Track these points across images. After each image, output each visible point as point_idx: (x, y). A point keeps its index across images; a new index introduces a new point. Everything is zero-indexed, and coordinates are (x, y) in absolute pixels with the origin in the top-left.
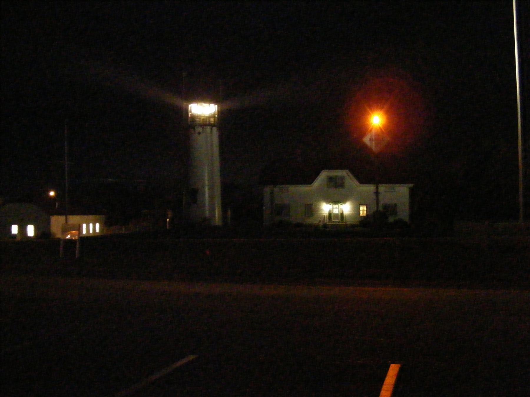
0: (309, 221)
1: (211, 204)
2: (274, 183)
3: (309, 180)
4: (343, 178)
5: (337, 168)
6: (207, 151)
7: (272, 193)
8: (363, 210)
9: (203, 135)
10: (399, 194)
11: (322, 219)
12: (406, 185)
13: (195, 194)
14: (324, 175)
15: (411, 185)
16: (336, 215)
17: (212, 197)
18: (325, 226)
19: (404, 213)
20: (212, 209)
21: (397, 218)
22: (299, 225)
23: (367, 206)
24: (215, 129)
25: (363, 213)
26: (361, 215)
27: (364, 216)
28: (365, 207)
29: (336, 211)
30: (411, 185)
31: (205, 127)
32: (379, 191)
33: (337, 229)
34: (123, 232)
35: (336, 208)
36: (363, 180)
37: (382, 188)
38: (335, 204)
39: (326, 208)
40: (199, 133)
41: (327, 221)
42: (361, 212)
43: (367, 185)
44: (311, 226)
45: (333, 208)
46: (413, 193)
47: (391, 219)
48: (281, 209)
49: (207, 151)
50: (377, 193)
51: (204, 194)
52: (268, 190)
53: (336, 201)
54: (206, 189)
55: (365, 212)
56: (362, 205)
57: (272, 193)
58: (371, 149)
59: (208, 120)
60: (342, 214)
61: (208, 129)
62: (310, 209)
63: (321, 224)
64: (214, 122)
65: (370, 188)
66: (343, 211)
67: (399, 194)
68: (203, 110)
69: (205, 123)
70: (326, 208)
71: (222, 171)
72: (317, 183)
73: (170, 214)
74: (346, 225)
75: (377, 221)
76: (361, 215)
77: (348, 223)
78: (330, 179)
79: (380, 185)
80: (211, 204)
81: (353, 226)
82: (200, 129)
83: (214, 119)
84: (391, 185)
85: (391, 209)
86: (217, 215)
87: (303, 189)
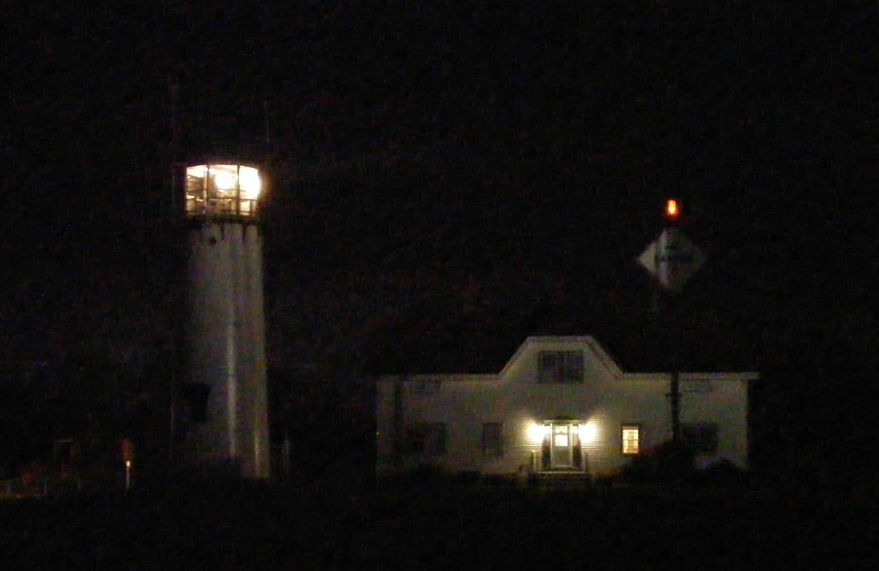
0: (501, 467)
1: (241, 423)
2: (403, 370)
3: (495, 363)
4: (579, 358)
5: (570, 333)
6: (232, 292)
7: (398, 392)
8: (631, 439)
9: (224, 248)
10: (723, 398)
11: (527, 462)
12: (737, 376)
13: (200, 398)
14: (531, 348)
15: (754, 376)
16: (562, 453)
17: (243, 406)
18: (534, 480)
19: (735, 443)
20: (244, 430)
21: (716, 459)
22: (468, 478)
23: (641, 427)
24: (253, 231)
25: (630, 447)
26: (625, 451)
27: (633, 455)
28: (636, 431)
29: (562, 441)
30: (754, 376)
31: (227, 227)
32: (680, 391)
33: (566, 488)
34: (8, 495)
35: (561, 433)
36: (630, 362)
37: (688, 382)
38: (559, 424)
39: (535, 434)
40: (213, 241)
41: (538, 467)
42: (626, 444)
43: (645, 375)
44: (497, 480)
45: (554, 435)
46: (755, 391)
47: (703, 462)
48: (419, 438)
49: (232, 292)
50: (674, 396)
51: (224, 393)
52: (386, 386)
53: (561, 418)
54: (232, 386)
55: (636, 444)
56: (631, 425)
57: (398, 392)
58: (655, 280)
59: (233, 207)
60: (577, 450)
61: (238, 229)
62: (497, 437)
63: (524, 474)
64: (251, 212)
65: (659, 383)
66: (579, 442)
67: (723, 398)
68: (239, 183)
69: (228, 217)
70: (535, 434)
71: (268, 336)
72: (513, 369)
73: (127, 445)
74: (587, 479)
75: (672, 457)
76: (625, 451)
77: (593, 472)
78: (546, 360)
79: (683, 376)
80: (241, 423)
81: (605, 481)
82: (214, 231)
83: (251, 206)
84: (705, 376)
85: (706, 436)
86: (257, 451)
87: (472, 384)
